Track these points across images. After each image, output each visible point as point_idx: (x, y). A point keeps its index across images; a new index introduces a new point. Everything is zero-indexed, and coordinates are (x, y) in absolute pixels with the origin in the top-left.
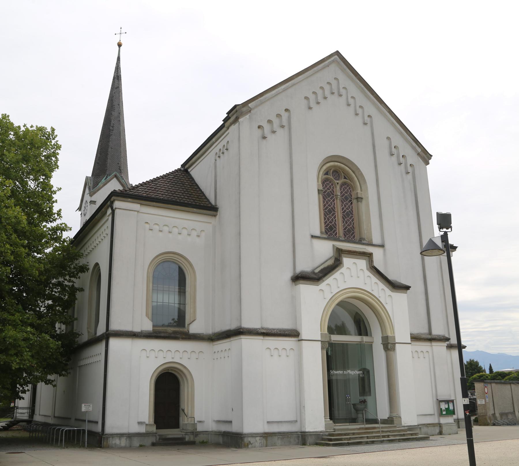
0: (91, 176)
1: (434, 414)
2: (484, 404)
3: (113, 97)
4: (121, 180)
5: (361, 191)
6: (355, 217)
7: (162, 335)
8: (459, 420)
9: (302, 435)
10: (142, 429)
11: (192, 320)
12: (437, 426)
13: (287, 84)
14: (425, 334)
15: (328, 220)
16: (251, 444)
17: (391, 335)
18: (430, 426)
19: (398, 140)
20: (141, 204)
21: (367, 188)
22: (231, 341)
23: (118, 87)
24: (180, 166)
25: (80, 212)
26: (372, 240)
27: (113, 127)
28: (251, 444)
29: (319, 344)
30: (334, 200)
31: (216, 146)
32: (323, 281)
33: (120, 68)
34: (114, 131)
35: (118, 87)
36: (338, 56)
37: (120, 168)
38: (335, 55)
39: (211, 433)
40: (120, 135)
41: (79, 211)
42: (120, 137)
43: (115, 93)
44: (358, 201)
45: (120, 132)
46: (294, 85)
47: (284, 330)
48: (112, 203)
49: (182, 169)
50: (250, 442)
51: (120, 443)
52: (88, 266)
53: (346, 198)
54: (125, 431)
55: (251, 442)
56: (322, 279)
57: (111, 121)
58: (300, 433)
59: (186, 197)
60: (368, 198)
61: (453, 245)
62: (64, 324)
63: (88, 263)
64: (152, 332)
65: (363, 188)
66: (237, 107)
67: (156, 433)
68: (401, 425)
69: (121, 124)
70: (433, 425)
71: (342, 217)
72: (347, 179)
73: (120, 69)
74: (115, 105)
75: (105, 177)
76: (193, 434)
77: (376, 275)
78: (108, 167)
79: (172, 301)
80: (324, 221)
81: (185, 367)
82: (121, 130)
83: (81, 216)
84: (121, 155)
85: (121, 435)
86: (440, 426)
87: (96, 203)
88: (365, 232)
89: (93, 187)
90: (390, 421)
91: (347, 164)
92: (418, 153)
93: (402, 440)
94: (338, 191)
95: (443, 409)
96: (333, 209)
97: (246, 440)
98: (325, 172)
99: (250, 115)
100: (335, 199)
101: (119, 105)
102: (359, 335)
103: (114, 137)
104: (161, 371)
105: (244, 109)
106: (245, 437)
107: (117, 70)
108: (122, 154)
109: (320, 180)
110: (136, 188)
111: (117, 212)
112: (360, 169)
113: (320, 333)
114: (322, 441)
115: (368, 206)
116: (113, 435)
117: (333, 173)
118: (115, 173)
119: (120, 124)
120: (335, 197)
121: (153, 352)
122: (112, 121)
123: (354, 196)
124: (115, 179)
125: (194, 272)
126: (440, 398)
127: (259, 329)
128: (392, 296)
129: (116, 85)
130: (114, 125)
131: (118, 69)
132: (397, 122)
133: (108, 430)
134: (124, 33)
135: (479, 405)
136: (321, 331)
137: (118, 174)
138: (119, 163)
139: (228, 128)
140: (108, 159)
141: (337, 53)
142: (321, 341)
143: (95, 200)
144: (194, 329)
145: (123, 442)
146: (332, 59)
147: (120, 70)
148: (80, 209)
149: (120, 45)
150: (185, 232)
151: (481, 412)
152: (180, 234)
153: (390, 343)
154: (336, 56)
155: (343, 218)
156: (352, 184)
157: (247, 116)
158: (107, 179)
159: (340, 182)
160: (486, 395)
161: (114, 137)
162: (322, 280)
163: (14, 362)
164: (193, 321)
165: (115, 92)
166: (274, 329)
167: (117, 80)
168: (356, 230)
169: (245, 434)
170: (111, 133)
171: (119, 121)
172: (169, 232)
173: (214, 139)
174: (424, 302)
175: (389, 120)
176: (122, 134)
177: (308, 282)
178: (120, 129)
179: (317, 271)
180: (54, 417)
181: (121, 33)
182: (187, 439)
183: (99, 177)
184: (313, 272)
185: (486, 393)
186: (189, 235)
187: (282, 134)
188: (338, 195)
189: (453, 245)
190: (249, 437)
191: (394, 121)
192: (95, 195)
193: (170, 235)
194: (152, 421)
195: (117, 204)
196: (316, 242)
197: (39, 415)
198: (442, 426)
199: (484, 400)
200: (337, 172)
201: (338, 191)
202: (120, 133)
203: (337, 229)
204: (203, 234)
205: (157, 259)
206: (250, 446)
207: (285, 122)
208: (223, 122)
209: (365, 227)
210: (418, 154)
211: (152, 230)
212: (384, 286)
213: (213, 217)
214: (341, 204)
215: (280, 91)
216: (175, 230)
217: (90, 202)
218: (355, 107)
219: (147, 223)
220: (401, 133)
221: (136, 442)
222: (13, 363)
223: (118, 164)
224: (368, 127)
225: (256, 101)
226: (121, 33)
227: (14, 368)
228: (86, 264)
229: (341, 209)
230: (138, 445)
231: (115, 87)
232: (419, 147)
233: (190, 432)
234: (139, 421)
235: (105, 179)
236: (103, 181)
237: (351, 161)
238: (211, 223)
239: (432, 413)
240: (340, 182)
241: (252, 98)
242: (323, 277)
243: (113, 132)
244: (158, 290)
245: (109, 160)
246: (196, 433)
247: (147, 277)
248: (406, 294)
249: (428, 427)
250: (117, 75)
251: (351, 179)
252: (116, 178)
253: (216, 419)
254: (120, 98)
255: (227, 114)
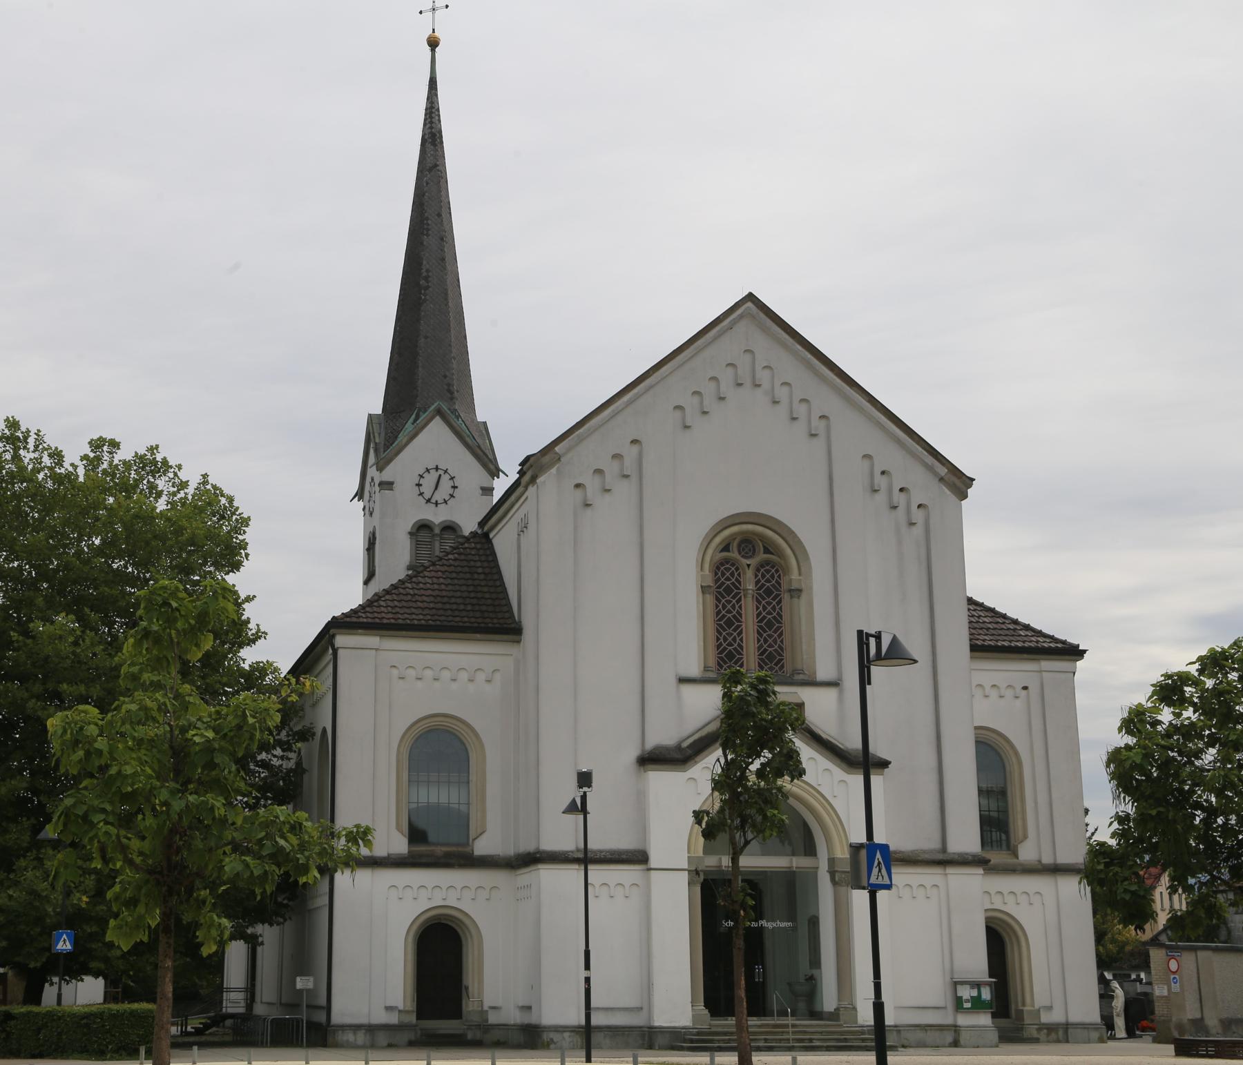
0: (381, 413)
1: (945, 1008)
2: (1166, 997)
3: (424, 195)
4: (453, 422)
5: (800, 574)
6: (786, 629)
7: (424, 860)
8: (1069, 1026)
9: (649, 1032)
10: (393, 1019)
11: (479, 831)
12: (949, 1030)
13: (636, 391)
14: (931, 851)
15: (725, 639)
16: (555, 1043)
17: (841, 856)
18: (931, 1030)
19: (890, 456)
20: (381, 636)
21: (810, 567)
22: (531, 871)
23: (436, 165)
24: (477, 526)
25: (361, 504)
26: (815, 673)
27: (426, 278)
28: (555, 1043)
29: (684, 877)
30: (740, 600)
31: (518, 509)
32: (696, 763)
33: (438, 110)
34: (430, 289)
35: (436, 165)
36: (753, 302)
37: (451, 388)
38: (746, 302)
39: (513, 1027)
40: (446, 299)
41: (359, 501)
42: (447, 305)
43: (427, 184)
44: (792, 597)
45: (446, 290)
46: (651, 387)
47: (620, 852)
48: (333, 636)
49: (479, 532)
50: (552, 1040)
51: (355, 1040)
52: (313, 728)
53: (768, 592)
54: (363, 1020)
55: (555, 1040)
56: (694, 759)
57: (422, 263)
58: (647, 1029)
59: (469, 608)
60: (811, 588)
61: (1078, 646)
62: (138, 948)
63: (311, 724)
64: (406, 856)
65: (803, 569)
66: (532, 459)
67: (416, 1026)
68: (857, 1023)
69: (449, 268)
70: (940, 1028)
71: (756, 630)
72: (773, 554)
73: (439, 111)
74: (429, 217)
75: (413, 416)
76: (480, 1029)
77: (814, 745)
78: (419, 389)
79: (454, 799)
80: (717, 644)
81: (466, 914)
82: (448, 282)
83: (365, 514)
84: (451, 352)
85: (356, 1028)
86: (955, 1031)
87: (394, 486)
88: (805, 657)
89: (385, 444)
90: (834, 1016)
91: (768, 525)
92: (940, 477)
93: (833, 1049)
94: (749, 582)
95: (964, 998)
96: (738, 617)
97: (546, 1037)
98: (721, 547)
99: (558, 467)
100: (743, 597)
101: (441, 215)
102: (805, 855)
103: (432, 306)
104: (419, 927)
105: (546, 459)
106: (543, 1031)
107: (431, 117)
108: (454, 350)
109: (707, 566)
110: (377, 601)
111: (340, 652)
112: (796, 532)
113: (687, 855)
114: (684, 1043)
115: (810, 605)
116: (344, 1027)
117: (739, 546)
118: (436, 405)
119: (445, 268)
120: (742, 594)
121: (423, 890)
122: (424, 262)
123: (785, 586)
124: (438, 419)
125: (482, 746)
126: (958, 977)
127: (572, 852)
128: (848, 782)
129: (430, 162)
130: (430, 274)
131: (433, 115)
132: (888, 419)
133: (336, 1018)
134: (441, 8)
135: (1158, 997)
136: (689, 853)
137: (445, 407)
138: (447, 374)
139: (526, 488)
140: (418, 367)
141: (751, 297)
142: (689, 871)
143: (391, 480)
144: (482, 847)
145: (361, 1038)
146: (739, 312)
147: (437, 118)
148: (360, 494)
149: (433, 43)
150: (464, 676)
151: (1161, 1012)
152: (454, 680)
153: (837, 871)
154: (749, 304)
155: (758, 633)
156: (782, 562)
157: (554, 471)
158: (418, 422)
159: (753, 562)
160: (1172, 977)
161: (432, 306)
162: (693, 762)
163: (184, 913)
164: (481, 834)
165: (429, 181)
166: (601, 851)
167: (432, 147)
168: (787, 655)
169: (545, 1027)
170: (423, 297)
171: (443, 259)
172: (435, 679)
173: (513, 498)
174: (933, 787)
175: (870, 418)
176: (450, 294)
177: (666, 767)
178: (446, 281)
179: (685, 745)
180: (281, 1003)
181: (434, 10)
182: (470, 1036)
183: (400, 416)
184: (678, 747)
185: (1174, 973)
186: (471, 680)
187: (624, 492)
188: (748, 589)
189: (1078, 646)
190: (551, 1031)
191: (883, 417)
192: (389, 466)
193: (437, 684)
194: (411, 1005)
195: (341, 640)
196: (687, 689)
197: (261, 1002)
198: (959, 1030)
199: (1166, 987)
200: (747, 544)
201: (749, 582)
202: (446, 294)
203: (745, 657)
204: (498, 676)
205: (415, 728)
206: (552, 1046)
207: (629, 464)
208: (518, 475)
209: (804, 647)
210: (941, 479)
211: (403, 678)
212: (831, 764)
213: (515, 644)
214: (755, 605)
215: (620, 408)
216: (446, 675)
217: (379, 485)
218: (791, 403)
219: (394, 666)
220: (899, 441)
221: (382, 1038)
222: (184, 915)
223: (445, 377)
224: (820, 443)
225: (569, 438)
226: (434, 10)
227: (185, 922)
228: (309, 725)
229: (755, 616)
230: (385, 1044)
231: (428, 168)
232: (943, 464)
233: (476, 1025)
234: (387, 1005)
235: (415, 421)
236: (409, 426)
237: (776, 519)
238: (512, 655)
239: (941, 1004)
240: (753, 562)
241: (571, 428)
242: (694, 755)
243: (427, 291)
244: (418, 782)
245: (420, 369)
246: (486, 1027)
247: (398, 761)
248: (881, 777)
249: (926, 1030)
250: (429, 130)
251: (781, 555)
252: (440, 417)
253: (520, 1005)
254: (441, 196)
255: (520, 465)
